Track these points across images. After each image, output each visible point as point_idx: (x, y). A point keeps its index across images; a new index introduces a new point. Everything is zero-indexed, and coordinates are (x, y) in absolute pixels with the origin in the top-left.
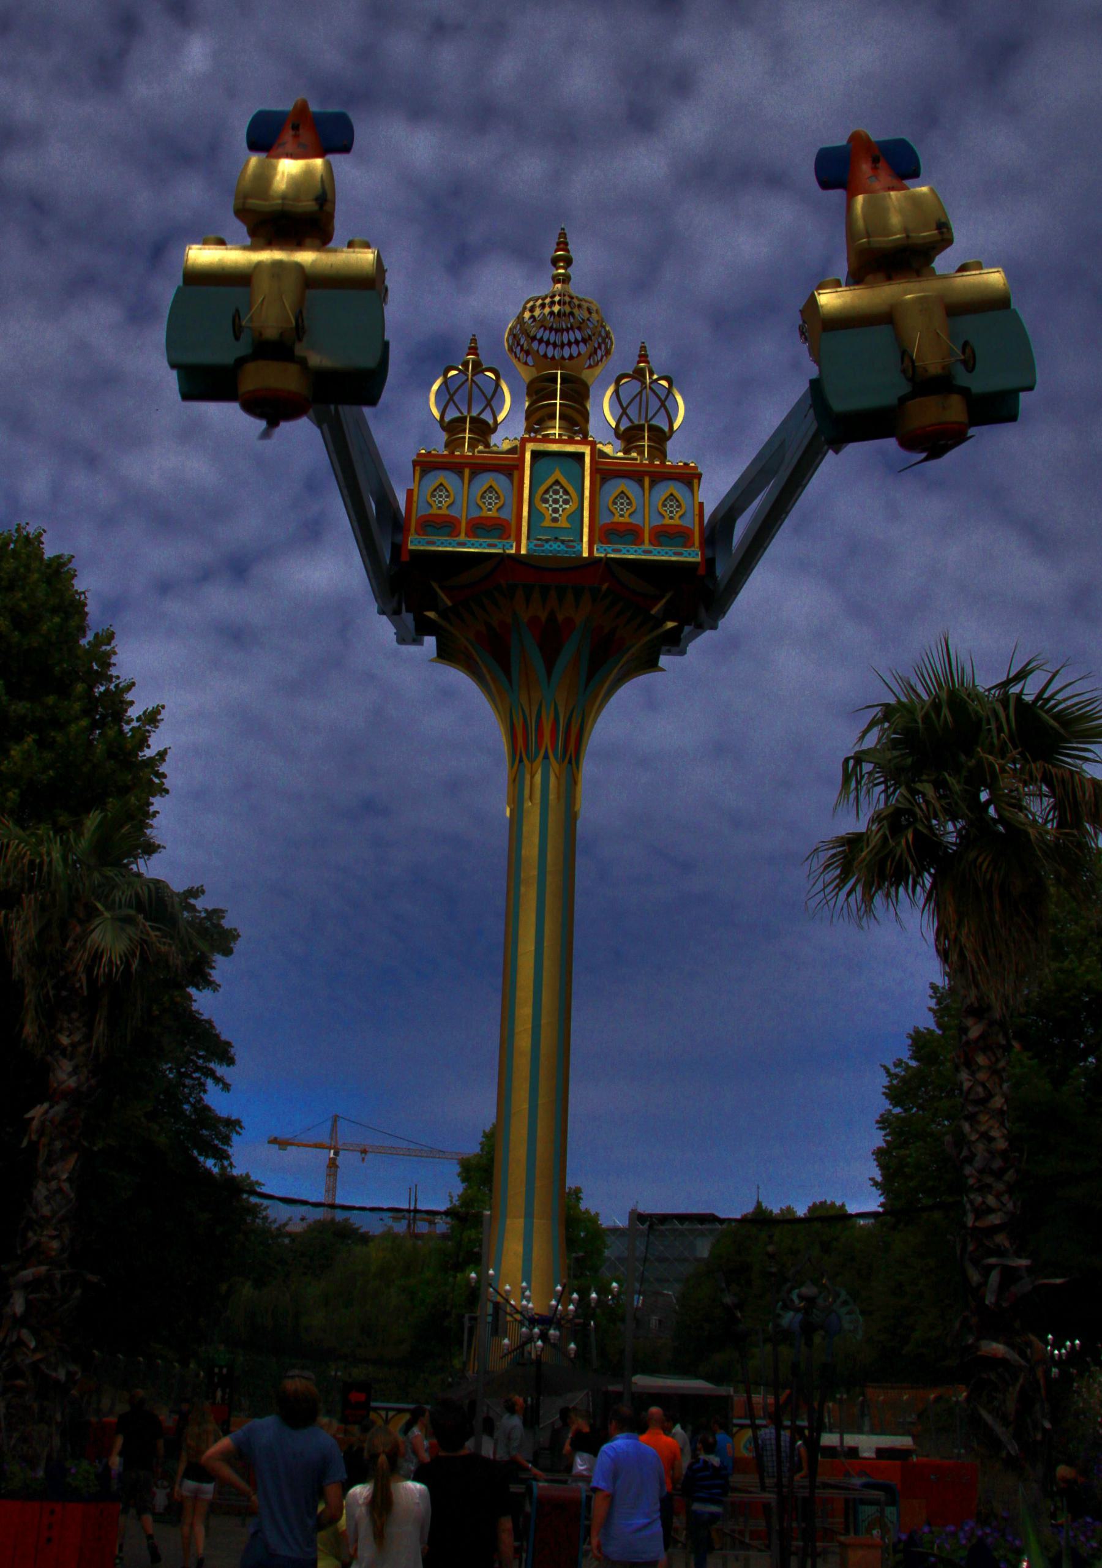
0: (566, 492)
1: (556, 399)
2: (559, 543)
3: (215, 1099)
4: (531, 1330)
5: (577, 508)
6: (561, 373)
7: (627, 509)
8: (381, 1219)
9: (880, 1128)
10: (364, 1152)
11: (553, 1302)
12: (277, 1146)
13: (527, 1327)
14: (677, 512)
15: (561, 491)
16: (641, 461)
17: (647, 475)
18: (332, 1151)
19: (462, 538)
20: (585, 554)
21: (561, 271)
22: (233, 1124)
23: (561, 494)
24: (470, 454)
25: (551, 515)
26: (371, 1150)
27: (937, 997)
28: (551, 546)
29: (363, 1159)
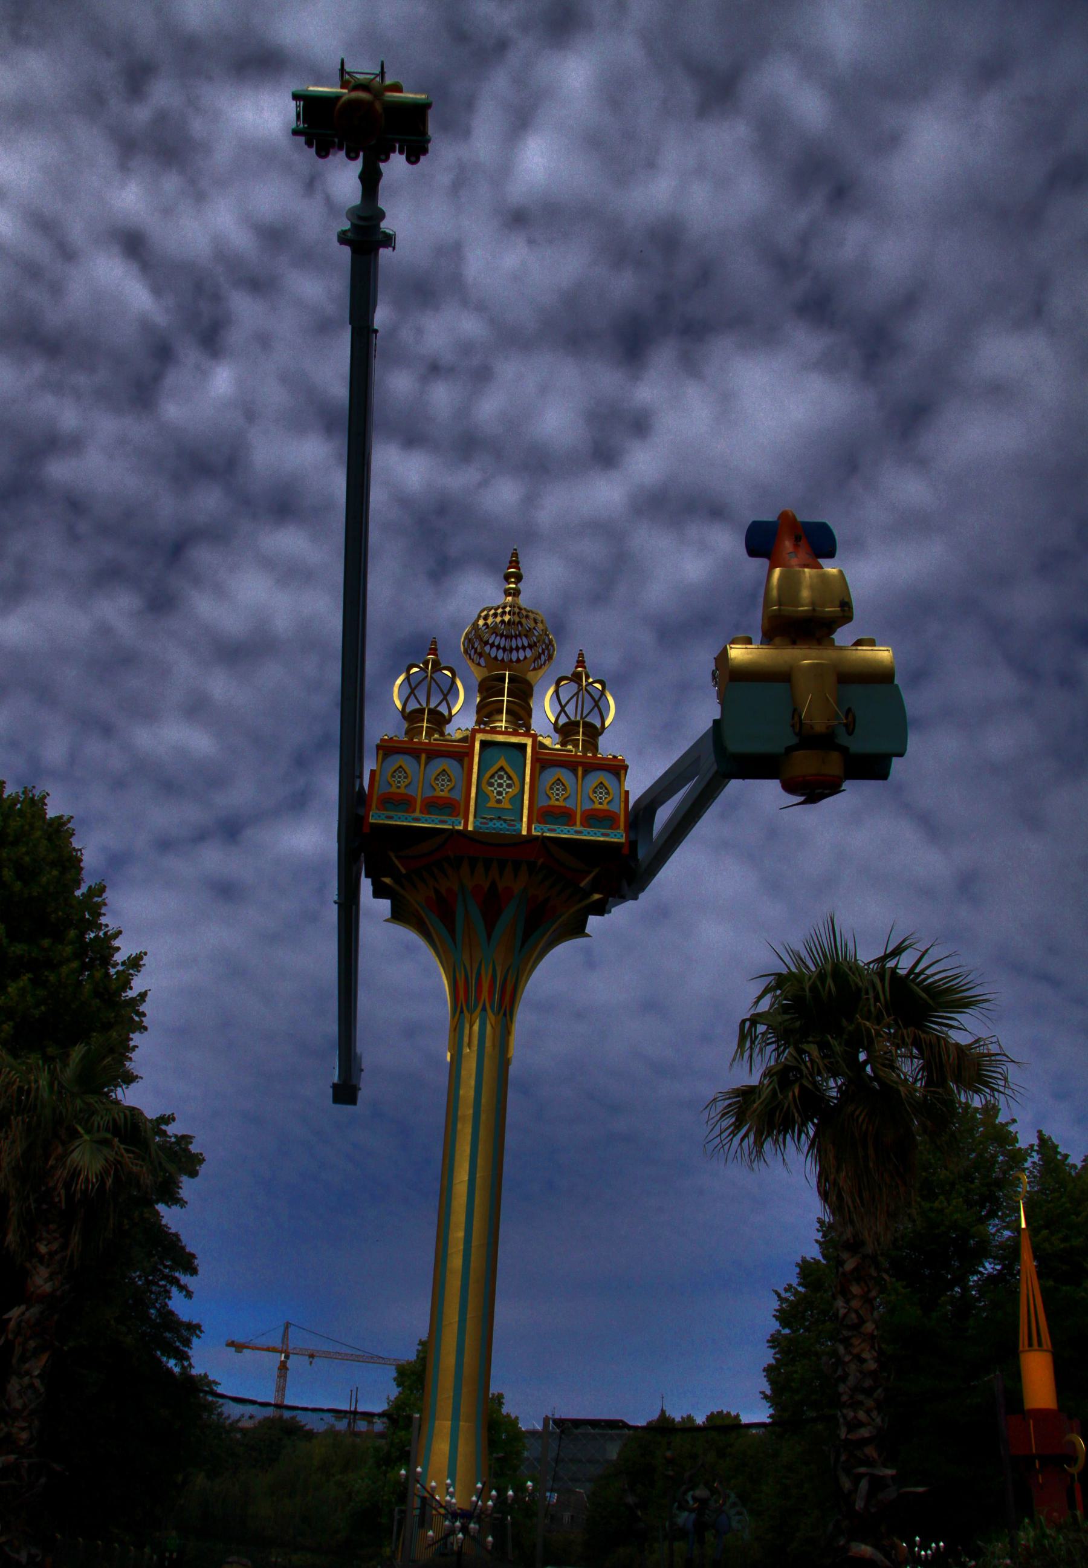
0: (509, 778)
1: (504, 697)
2: (502, 822)
3: (177, 1304)
4: (453, 1523)
5: (519, 791)
6: (509, 674)
7: (562, 794)
8: (322, 1419)
9: (771, 1347)
10: (312, 1356)
11: (474, 1498)
12: (234, 1349)
13: (450, 1521)
14: (606, 798)
15: (505, 776)
16: (576, 753)
17: (580, 765)
18: (283, 1355)
19: (417, 814)
20: (524, 832)
21: (513, 586)
22: (194, 1328)
23: (505, 779)
24: (427, 741)
25: (495, 797)
26: (318, 1355)
27: (822, 1231)
28: (495, 824)
29: (311, 1363)
